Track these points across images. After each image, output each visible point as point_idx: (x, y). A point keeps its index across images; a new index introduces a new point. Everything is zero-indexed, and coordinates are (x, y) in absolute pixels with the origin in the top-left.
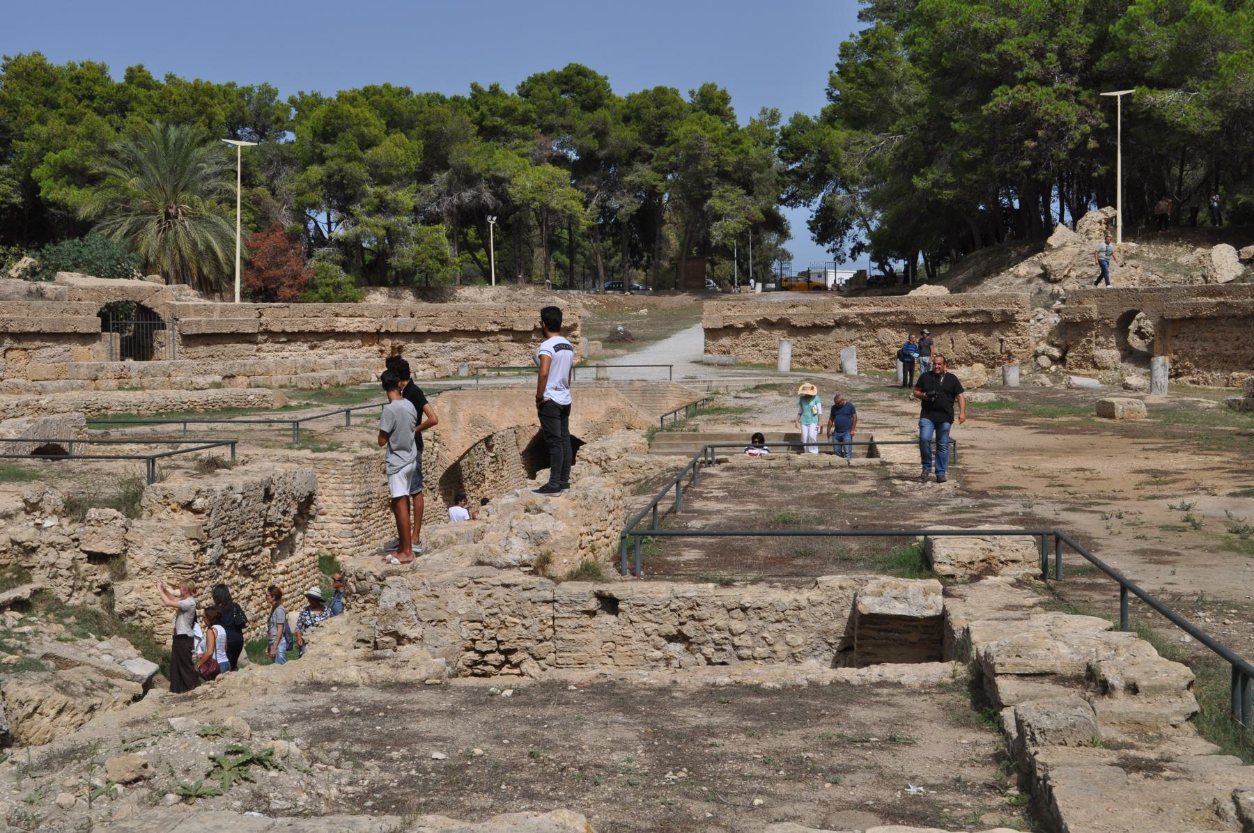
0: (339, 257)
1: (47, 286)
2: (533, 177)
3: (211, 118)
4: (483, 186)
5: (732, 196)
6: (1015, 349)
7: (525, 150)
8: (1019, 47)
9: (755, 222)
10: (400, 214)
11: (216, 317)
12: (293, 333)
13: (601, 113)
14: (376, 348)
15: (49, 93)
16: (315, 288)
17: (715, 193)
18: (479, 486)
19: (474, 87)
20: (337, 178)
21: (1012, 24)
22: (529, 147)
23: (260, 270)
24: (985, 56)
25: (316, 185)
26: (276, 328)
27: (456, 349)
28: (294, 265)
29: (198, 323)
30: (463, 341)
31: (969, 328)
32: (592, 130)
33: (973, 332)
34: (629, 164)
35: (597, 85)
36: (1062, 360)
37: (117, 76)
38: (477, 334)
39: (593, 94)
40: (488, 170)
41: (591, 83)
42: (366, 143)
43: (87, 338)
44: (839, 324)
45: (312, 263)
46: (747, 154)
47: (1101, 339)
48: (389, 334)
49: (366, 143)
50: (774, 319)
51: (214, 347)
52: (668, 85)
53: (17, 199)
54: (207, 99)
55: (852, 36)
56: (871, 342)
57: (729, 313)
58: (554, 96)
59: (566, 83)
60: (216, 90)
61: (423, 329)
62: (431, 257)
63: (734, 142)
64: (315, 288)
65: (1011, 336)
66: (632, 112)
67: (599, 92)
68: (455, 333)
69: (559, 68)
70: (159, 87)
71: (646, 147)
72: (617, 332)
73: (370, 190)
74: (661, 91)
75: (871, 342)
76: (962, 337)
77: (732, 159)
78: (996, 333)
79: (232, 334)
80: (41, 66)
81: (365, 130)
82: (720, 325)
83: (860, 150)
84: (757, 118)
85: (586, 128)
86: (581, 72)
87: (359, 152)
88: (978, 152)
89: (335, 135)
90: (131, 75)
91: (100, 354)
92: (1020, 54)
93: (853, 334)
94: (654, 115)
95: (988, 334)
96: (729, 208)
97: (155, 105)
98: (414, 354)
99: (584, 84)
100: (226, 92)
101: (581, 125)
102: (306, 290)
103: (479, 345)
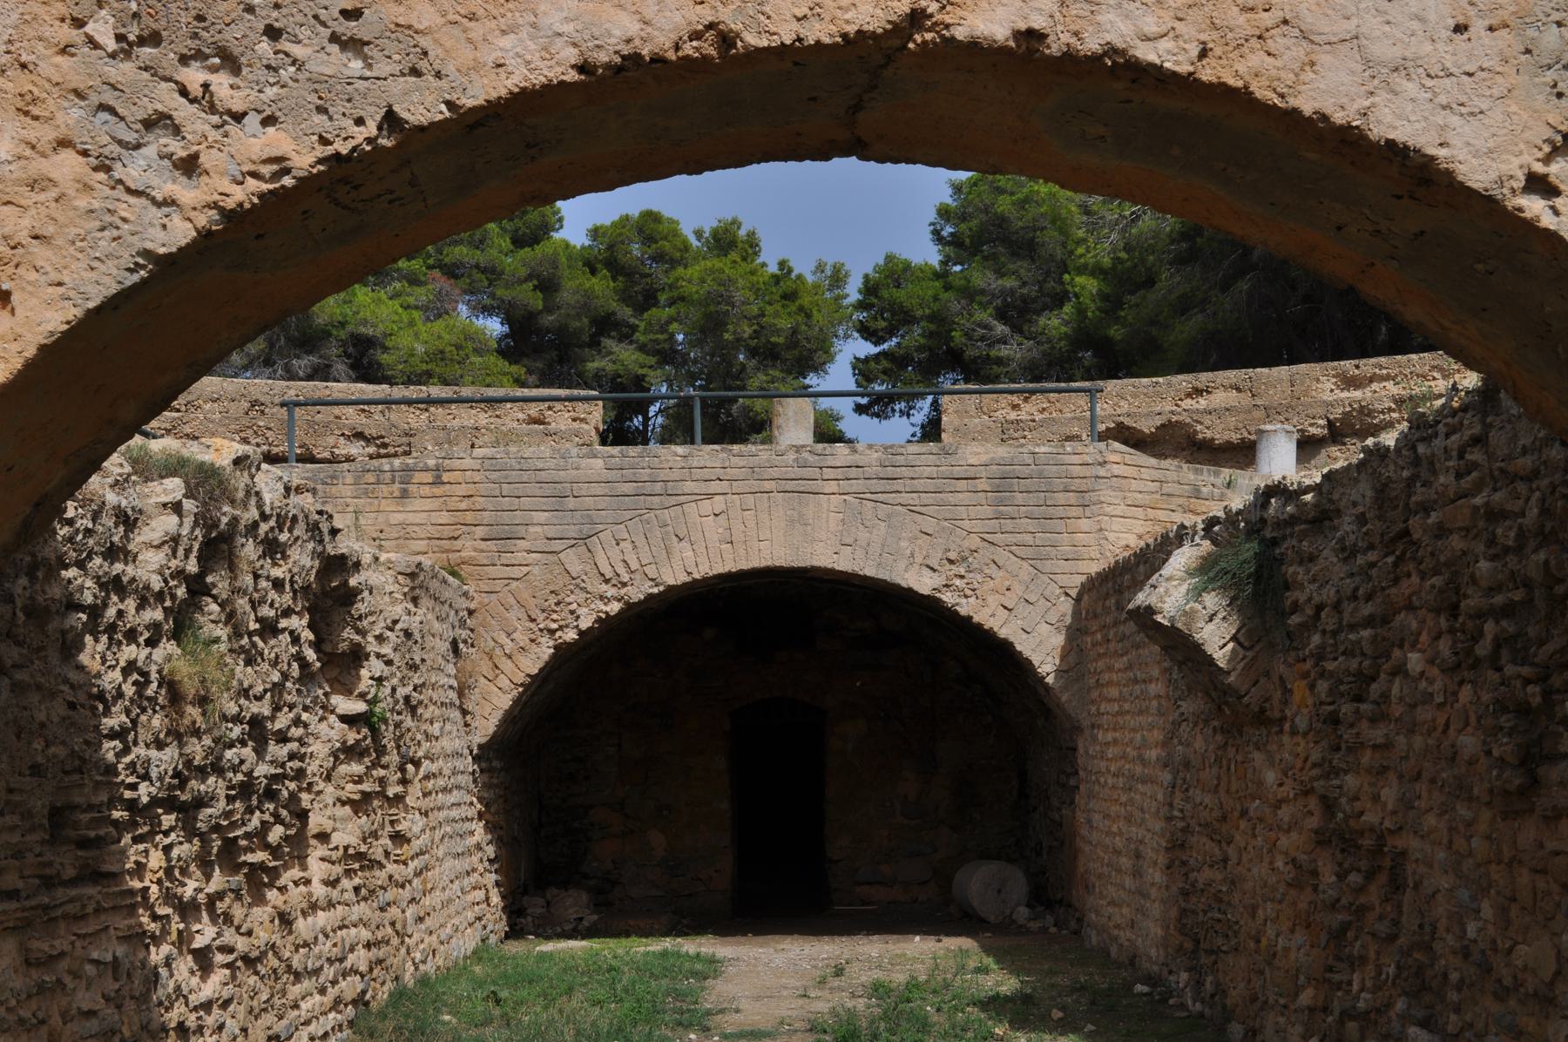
7: (411, 300)
18: (259, 881)
32: (529, 277)
46: (809, 316)
63: (785, 297)
71: (625, 313)
77: (785, 323)
85: (523, 272)
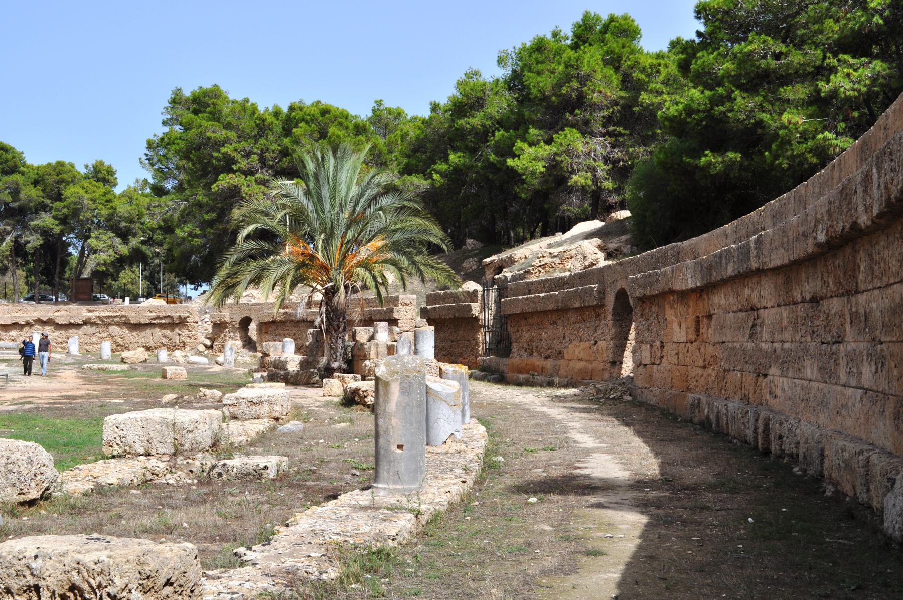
5: (105, 238)
6: (187, 340)
8: (236, 150)
9: (121, 256)
13: (16, 177)
17: (93, 235)
21: (232, 135)
24: (215, 154)
31: (162, 326)
33: (164, 328)
34: (36, 212)
35: (14, 157)
36: (211, 347)
39: (11, 163)
41: (9, 156)
44: (85, 323)
47: (232, 334)
50: (45, 319)
52: (67, 160)
55: (155, 136)
56: (105, 335)
57: (16, 314)
60: (270, 119)
63: (107, 201)
65: (185, 332)
67: (15, 162)
74: (60, 164)
75: (105, 335)
76: (158, 332)
77: (105, 212)
78: (177, 330)
82: (9, 322)
83: (157, 210)
88: (214, 215)
92: (235, 154)
93: (94, 329)
95: (172, 330)
96: (101, 245)
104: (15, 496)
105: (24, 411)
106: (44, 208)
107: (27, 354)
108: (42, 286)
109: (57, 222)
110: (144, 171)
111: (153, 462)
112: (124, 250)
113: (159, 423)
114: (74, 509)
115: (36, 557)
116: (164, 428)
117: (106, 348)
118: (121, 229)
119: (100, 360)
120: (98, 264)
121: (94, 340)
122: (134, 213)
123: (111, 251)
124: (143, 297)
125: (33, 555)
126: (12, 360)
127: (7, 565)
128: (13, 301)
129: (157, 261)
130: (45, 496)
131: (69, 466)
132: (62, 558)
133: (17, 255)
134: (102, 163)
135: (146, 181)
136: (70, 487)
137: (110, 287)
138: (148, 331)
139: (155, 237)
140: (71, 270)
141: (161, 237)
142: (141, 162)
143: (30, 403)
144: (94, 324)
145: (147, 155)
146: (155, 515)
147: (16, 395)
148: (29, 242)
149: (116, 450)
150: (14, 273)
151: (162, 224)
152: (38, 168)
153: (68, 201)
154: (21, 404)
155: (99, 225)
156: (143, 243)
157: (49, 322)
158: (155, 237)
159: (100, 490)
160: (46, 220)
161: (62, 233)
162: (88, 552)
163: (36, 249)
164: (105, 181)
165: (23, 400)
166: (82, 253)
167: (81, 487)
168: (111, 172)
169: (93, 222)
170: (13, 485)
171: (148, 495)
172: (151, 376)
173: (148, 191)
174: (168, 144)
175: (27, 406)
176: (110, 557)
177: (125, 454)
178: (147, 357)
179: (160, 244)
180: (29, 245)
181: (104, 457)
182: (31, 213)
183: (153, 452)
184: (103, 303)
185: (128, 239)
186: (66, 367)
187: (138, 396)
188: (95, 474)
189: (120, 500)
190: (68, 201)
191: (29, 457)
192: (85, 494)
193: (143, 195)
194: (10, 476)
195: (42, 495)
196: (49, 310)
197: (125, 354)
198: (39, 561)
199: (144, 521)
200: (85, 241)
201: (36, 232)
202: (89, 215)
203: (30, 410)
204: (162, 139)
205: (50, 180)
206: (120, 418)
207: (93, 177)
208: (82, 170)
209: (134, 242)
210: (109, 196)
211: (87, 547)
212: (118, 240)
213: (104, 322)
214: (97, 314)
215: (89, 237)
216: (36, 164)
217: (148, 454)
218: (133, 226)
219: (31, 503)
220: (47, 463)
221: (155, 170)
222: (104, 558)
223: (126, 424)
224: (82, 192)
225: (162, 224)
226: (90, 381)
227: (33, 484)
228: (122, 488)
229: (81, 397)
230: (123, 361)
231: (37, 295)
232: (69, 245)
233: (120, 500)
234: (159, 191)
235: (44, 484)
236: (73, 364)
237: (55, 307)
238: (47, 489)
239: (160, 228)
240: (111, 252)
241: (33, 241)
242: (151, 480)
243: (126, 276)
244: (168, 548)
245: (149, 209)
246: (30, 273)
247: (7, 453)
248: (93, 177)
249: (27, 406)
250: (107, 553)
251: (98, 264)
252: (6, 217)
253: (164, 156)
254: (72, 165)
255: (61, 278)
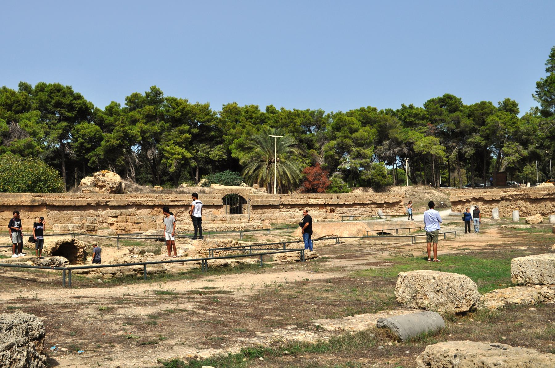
0: (341, 176)
1: (207, 189)
2: (425, 141)
3: (295, 124)
4: (404, 146)
5: (513, 146)
7: (423, 130)
9: (523, 157)
10: (366, 158)
11: (264, 199)
12: (293, 205)
13: (458, 114)
14: (324, 210)
15: (237, 117)
16: (331, 188)
17: (505, 145)
19: (403, 106)
20: (341, 145)
22: (425, 129)
23: (310, 182)
25: (333, 148)
26: (286, 203)
27: (355, 210)
28: (323, 179)
29: (257, 201)
30: (358, 207)
34: (470, 134)
35: (456, 102)
37: (263, 110)
38: (363, 205)
39: (454, 106)
40: (406, 139)
41: (453, 102)
42: (353, 131)
43: (218, 207)
45: (331, 178)
48: (329, 205)
49: (353, 131)
50: (477, 198)
51: (264, 210)
53: (225, 157)
54: (293, 117)
55: (541, 79)
58: (437, 108)
59: (443, 102)
61: (342, 203)
62: (379, 175)
63: (513, 123)
64: (331, 188)
66: (472, 113)
67: (456, 105)
68: (354, 204)
69: (441, 96)
70: (278, 112)
71: (477, 127)
72: (441, 204)
73: (354, 149)
74: (483, 103)
77: (512, 130)
79: (270, 205)
80: (235, 108)
81: (352, 126)
82: (457, 200)
83: (545, 126)
84: (529, 112)
86: (449, 97)
87: (349, 135)
89: (340, 129)
90: (268, 109)
91: (223, 212)
93: (508, 203)
94: (481, 112)
96: (511, 151)
97: (275, 120)
98: (339, 212)
99: (450, 102)
100: (297, 114)
101: (448, 119)
102: (328, 189)
103: (364, 209)
104: (453, 309)
105: (464, 254)
106: (475, 131)
107: (467, 218)
108: (476, 178)
109: (483, 139)
110: (536, 102)
111: (545, 289)
112: (525, 153)
113: (548, 264)
114: (491, 318)
115: (455, 356)
116: (552, 267)
117: (516, 215)
118: (522, 140)
119: (512, 222)
120: (510, 163)
121: (508, 209)
122: (531, 129)
123: (517, 154)
124: (539, 182)
125: (453, 355)
126: (459, 223)
127: (437, 359)
128: (459, 188)
129: (547, 159)
130: (473, 310)
131: (489, 290)
132: (473, 359)
133: (460, 160)
134: (509, 100)
135: (537, 108)
136: (488, 304)
137: (518, 176)
138: (543, 204)
139: (545, 143)
140: (493, 167)
141: (549, 143)
142: (533, 97)
143: (468, 249)
144: (507, 200)
145: (537, 92)
146: (546, 327)
147: (460, 244)
148: (467, 152)
149: (520, 280)
150: (459, 171)
151: (549, 134)
152: (470, 107)
153: (489, 125)
154: (462, 249)
155: (509, 139)
156: (537, 147)
157: (481, 199)
158: (545, 143)
159: (509, 307)
160: (477, 138)
161: (486, 145)
162: (490, 356)
163: (471, 156)
164: (511, 111)
165: (464, 247)
166: (499, 156)
167: (496, 304)
168: (515, 105)
169: (505, 137)
170: (452, 302)
171: (542, 312)
172: (546, 232)
173: (539, 114)
174: (550, 83)
175: (467, 251)
176: (505, 361)
177: (527, 283)
178: (542, 220)
179: (548, 148)
180: (467, 154)
181: (513, 285)
182: (467, 135)
183: (545, 282)
184: (514, 187)
185: (528, 146)
186: (491, 227)
187: (536, 245)
188: (506, 296)
189: (522, 314)
190: (489, 125)
191: (461, 285)
192: (499, 309)
193: (536, 117)
194: (450, 296)
195: (470, 309)
196: (480, 192)
197: (528, 218)
198: (458, 359)
199: (538, 330)
200: (501, 149)
201: (470, 145)
202: (502, 133)
203: (468, 253)
204: (546, 81)
205: (477, 113)
206: (523, 259)
207: (504, 109)
208: (497, 106)
209: (531, 147)
210: (514, 120)
211: (490, 352)
212: (521, 147)
213: (514, 199)
214: (509, 193)
215: (503, 146)
216: (469, 105)
217: (541, 284)
218: (530, 137)
219: (464, 314)
220: (473, 289)
221: (543, 101)
222: (501, 362)
223: (525, 264)
224: (497, 119)
225: (549, 134)
226: (506, 236)
227: (464, 302)
228: (524, 307)
229: (500, 245)
230: (527, 222)
231: (473, 184)
232: (491, 152)
233: (522, 314)
234: (546, 114)
235: (472, 302)
236: (496, 225)
237: (483, 190)
238: (474, 305)
239: (548, 137)
240: (517, 155)
241: (469, 151)
242: (544, 301)
243: (527, 169)
244: (548, 358)
245: (540, 126)
246: (468, 170)
247: (448, 282)
248: (504, 109)
249: (467, 251)
250: (503, 358)
251: (510, 163)
252: (453, 138)
253: (548, 91)
254: (490, 103)
255: (487, 173)
